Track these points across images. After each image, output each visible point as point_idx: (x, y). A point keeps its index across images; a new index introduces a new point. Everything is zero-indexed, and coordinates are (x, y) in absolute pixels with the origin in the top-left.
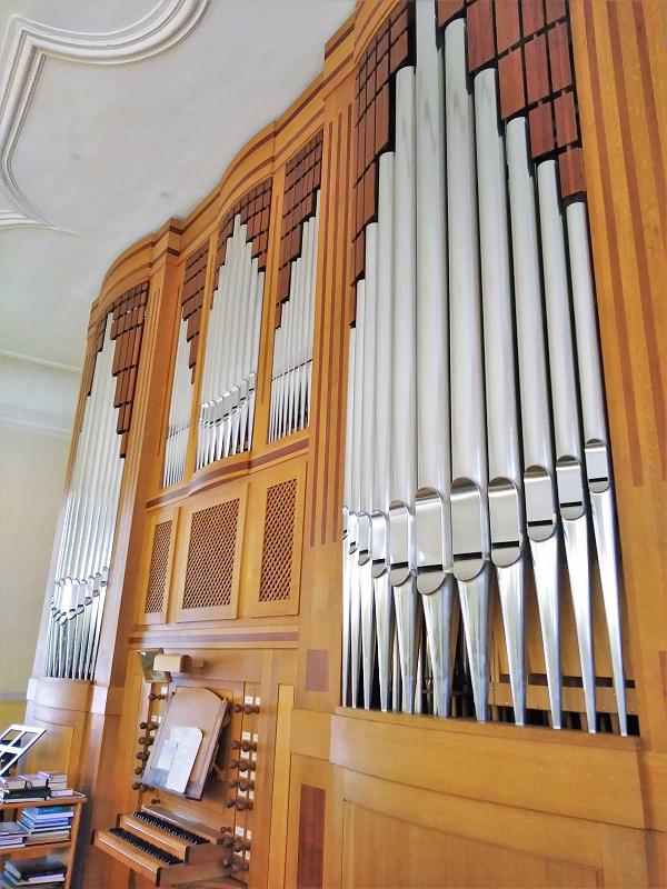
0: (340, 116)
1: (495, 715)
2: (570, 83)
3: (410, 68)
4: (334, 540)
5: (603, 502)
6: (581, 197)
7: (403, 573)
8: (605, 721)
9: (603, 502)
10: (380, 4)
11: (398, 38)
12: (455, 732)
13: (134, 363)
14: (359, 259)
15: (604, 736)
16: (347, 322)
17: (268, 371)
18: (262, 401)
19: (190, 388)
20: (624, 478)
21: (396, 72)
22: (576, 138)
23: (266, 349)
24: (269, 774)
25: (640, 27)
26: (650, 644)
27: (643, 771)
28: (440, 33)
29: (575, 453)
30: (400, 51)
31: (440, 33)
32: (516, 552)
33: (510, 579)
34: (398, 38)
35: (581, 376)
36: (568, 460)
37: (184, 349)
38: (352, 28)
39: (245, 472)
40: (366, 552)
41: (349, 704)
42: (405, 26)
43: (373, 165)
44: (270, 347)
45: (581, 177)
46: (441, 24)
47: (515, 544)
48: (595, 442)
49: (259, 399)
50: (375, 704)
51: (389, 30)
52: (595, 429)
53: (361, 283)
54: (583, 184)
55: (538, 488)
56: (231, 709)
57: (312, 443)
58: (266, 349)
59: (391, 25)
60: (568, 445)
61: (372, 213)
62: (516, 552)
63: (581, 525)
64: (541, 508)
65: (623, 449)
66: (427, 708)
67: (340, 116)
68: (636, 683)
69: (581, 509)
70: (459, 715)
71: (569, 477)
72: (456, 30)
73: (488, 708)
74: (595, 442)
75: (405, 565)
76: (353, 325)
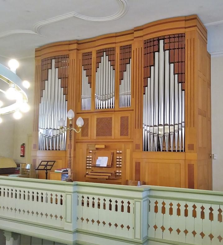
4: (141, 128)
5: (183, 129)
6: (184, 90)
16: (143, 92)
17: (118, 93)
18: (117, 99)
19: (90, 90)
23: (117, 89)
24: (125, 162)
25: (194, 45)
26: (187, 143)
27: (194, 239)
35: (188, 194)
37: (85, 79)
39: (114, 112)
44: (118, 89)
45: (184, 88)
49: (116, 98)
50: (147, 150)
55: (176, 126)
56: (113, 154)
57: (135, 110)
58: (117, 89)
66: (155, 151)
68: (109, 223)
71: (180, 125)
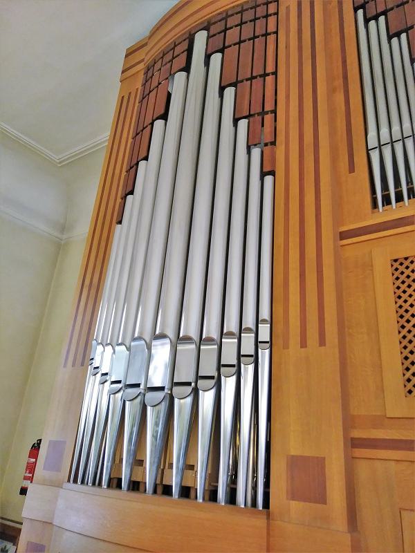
0: (130, 93)
1: (160, 490)
2: (273, 109)
3: (184, 74)
5: (264, 355)
6: (272, 173)
7: (133, 392)
8: (186, 492)
9: (264, 355)
10: (211, 3)
11: (178, 55)
12: (125, 500)
13: (270, 69)
14: (131, 182)
15: (185, 501)
20: (278, 342)
21: (175, 73)
22: (273, 140)
28: (208, 58)
29: (252, 326)
30: (181, 61)
31: (208, 58)
32: (212, 382)
33: (207, 399)
34: (178, 55)
36: (248, 330)
38: (146, 44)
40: (106, 374)
41: (75, 481)
42: (186, 47)
43: (149, 127)
45: (273, 161)
46: (209, 52)
47: (212, 378)
48: (264, 321)
51: (174, 49)
52: (265, 313)
53: (129, 197)
54: (275, 166)
55: (230, 344)
59: (175, 46)
60: (249, 321)
61: (145, 155)
62: (212, 382)
63: (251, 368)
64: (229, 357)
65: (279, 328)
67: (130, 93)
69: (252, 359)
70: (133, 490)
71: (248, 339)
72: (216, 59)
73: (110, 480)
74: (264, 321)
75: (138, 385)
76: (120, 222)
